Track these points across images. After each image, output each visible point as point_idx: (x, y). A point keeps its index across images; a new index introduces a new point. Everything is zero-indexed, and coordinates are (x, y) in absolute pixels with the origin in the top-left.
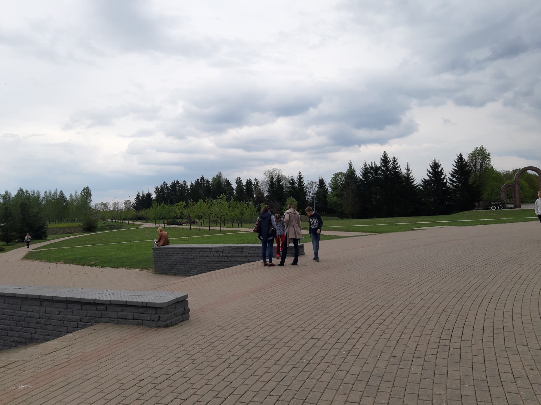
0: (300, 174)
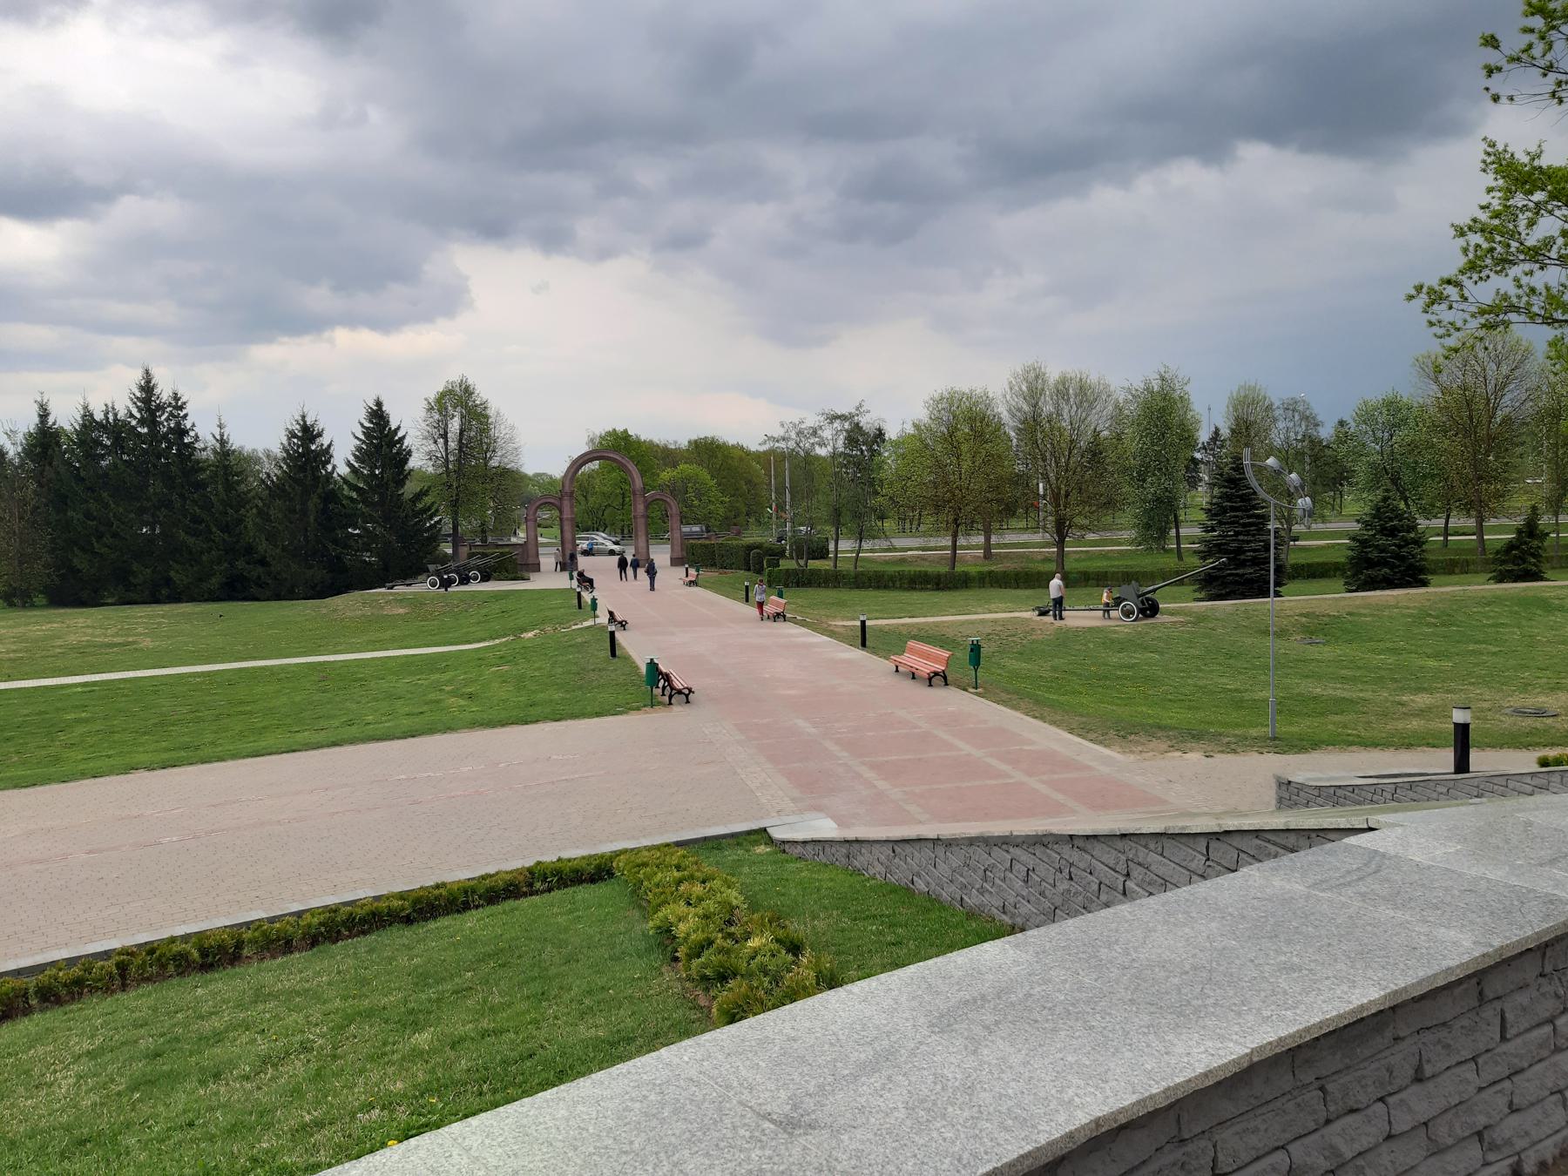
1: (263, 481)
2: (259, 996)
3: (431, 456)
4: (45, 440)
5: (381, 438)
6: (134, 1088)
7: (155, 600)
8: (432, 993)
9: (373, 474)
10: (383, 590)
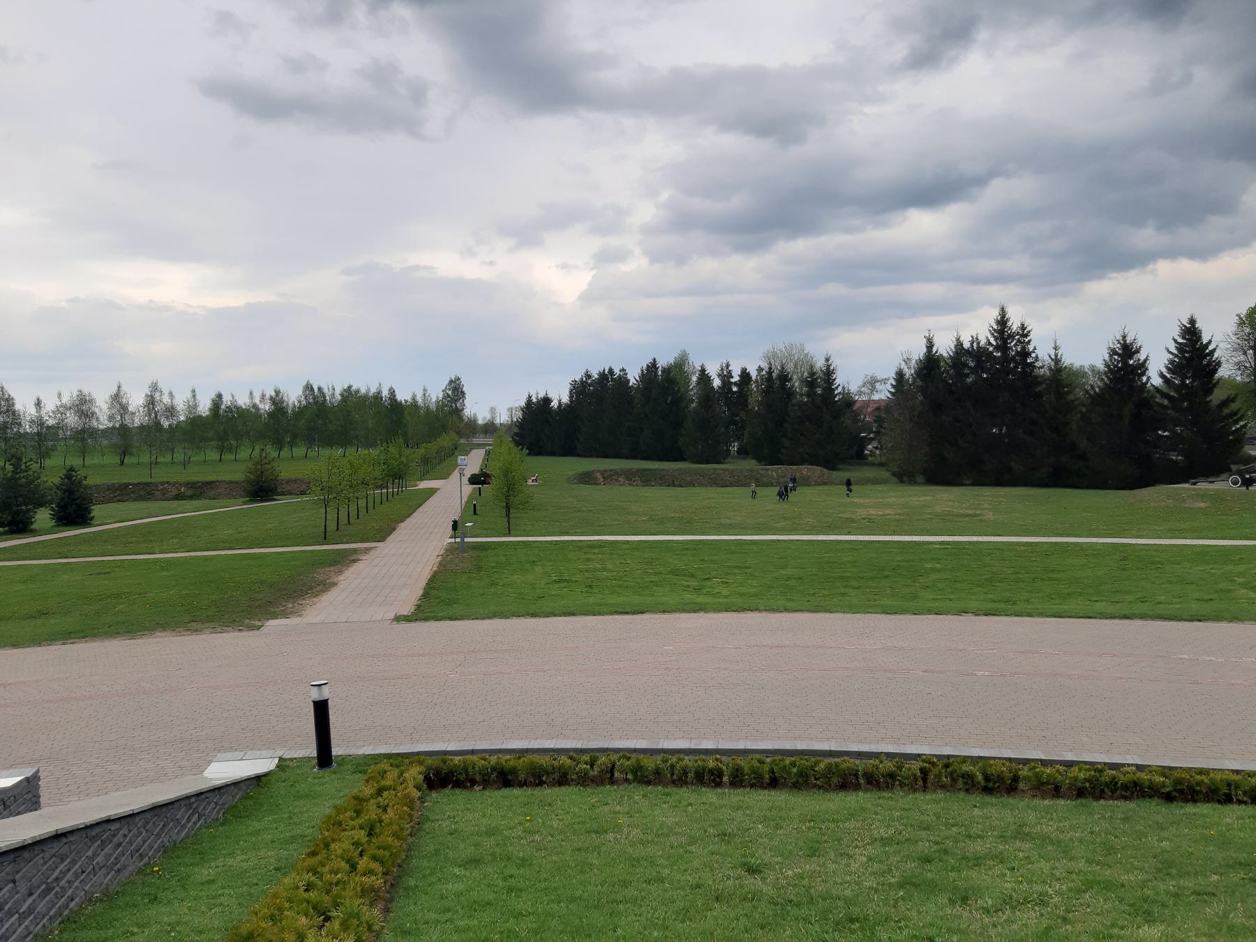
0: (827, 360)
1: (1087, 392)
2: (1021, 834)
3: (1239, 365)
4: (930, 363)
5: (1193, 353)
6: (901, 886)
7: (999, 483)
8: (1171, 885)
9: (1183, 384)
10: (1186, 485)
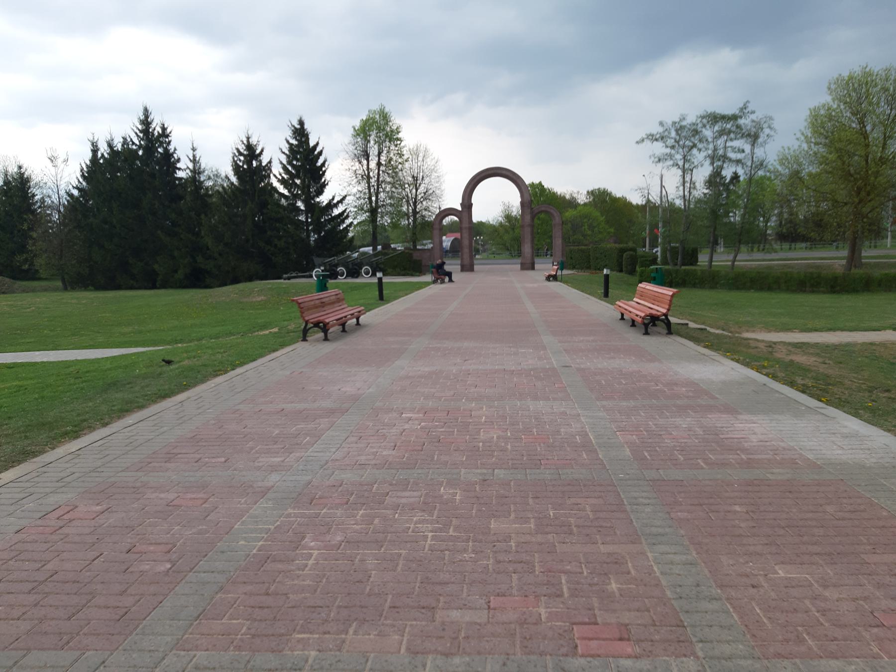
0: (20, 167)
